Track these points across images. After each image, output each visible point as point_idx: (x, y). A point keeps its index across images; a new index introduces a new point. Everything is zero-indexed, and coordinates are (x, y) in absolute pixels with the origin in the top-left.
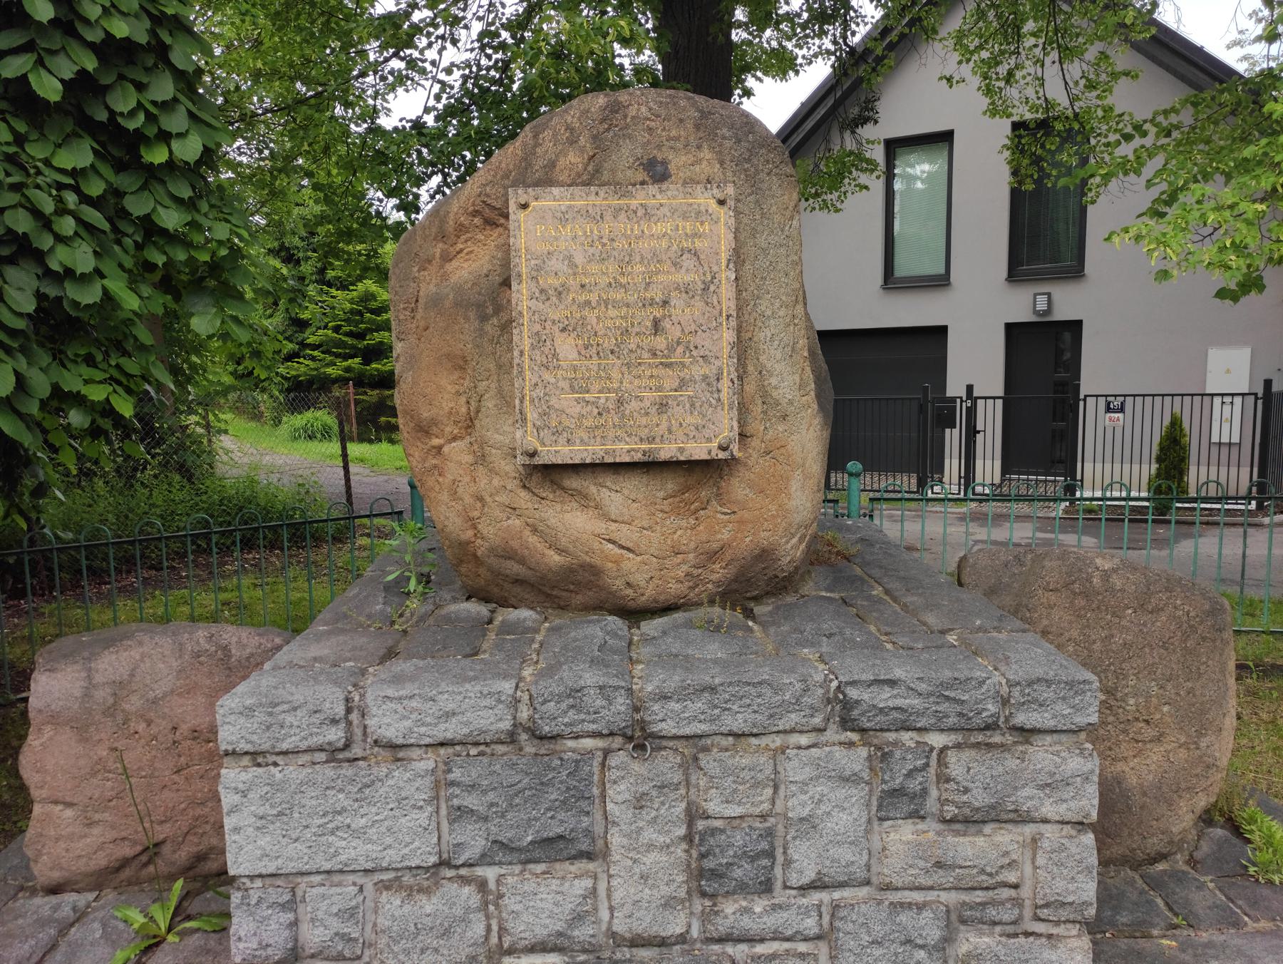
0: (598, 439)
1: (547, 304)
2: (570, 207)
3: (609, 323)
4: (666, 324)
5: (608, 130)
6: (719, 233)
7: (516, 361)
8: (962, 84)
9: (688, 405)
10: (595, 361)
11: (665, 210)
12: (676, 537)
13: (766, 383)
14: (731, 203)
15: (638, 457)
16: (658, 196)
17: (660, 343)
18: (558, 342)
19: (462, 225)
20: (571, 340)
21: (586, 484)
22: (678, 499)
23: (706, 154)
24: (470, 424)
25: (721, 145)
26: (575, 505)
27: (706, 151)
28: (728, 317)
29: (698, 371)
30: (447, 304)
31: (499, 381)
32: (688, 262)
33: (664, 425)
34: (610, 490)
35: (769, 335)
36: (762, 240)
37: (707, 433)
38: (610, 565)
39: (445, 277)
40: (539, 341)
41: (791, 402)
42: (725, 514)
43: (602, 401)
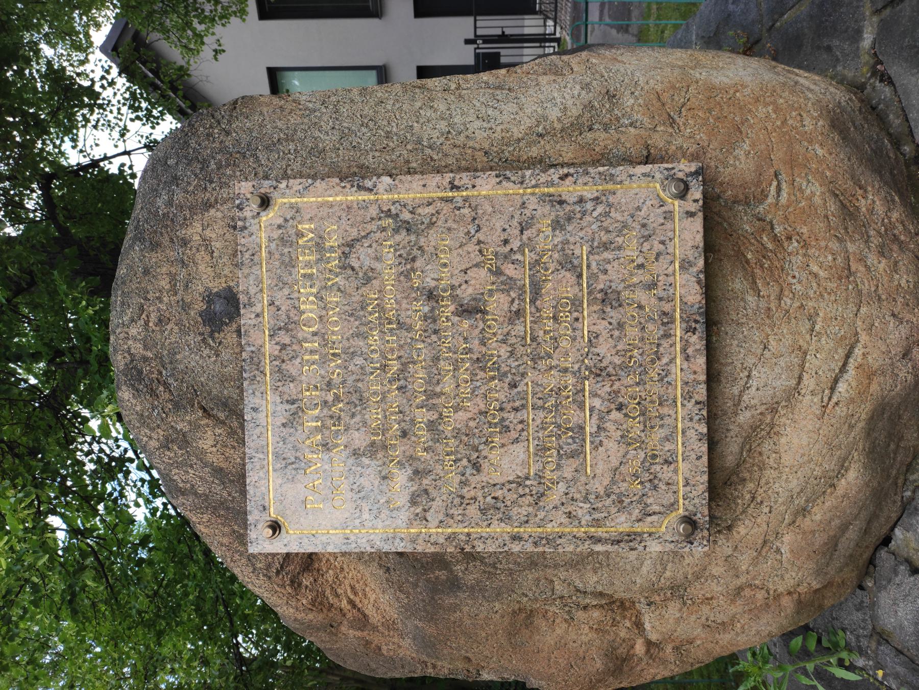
0: (665, 410)
1: (433, 493)
2: (277, 455)
3: (466, 389)
4: (466, 293)
5: (166, 385)
6: (316, 205)
7: (529, 547)
8: (221, 41)
9: (607, 255)
10: (529, 415)
11: (280, 297)
12: (822, 274)
13: (558, 126)
14: (266, 186)
15: (697, 341)
16: (258, 308)
17: (498, 304)
18: (497, 478)
19: (313, 602)
20: (494, 456)
21: (734, 429)
22: (758, 271)
23: (194, 231)
24: (618, 606)
25: (181, 207)
26: (767, 446)
27: (190, 231)
28: (454, 187)
29: (546, 237)
30: (431, 630)
31: (556, 566)
32: (362, 257)
33: (641, 296)
34: (746, 387)
35: (478, 123)
36: (328, 140)
37: (655, 218)
38: (874, 387)
39: (390, 625)
40: (494, 509)
41: (586, 86)
42: (779, 189)
43: (597, 403)
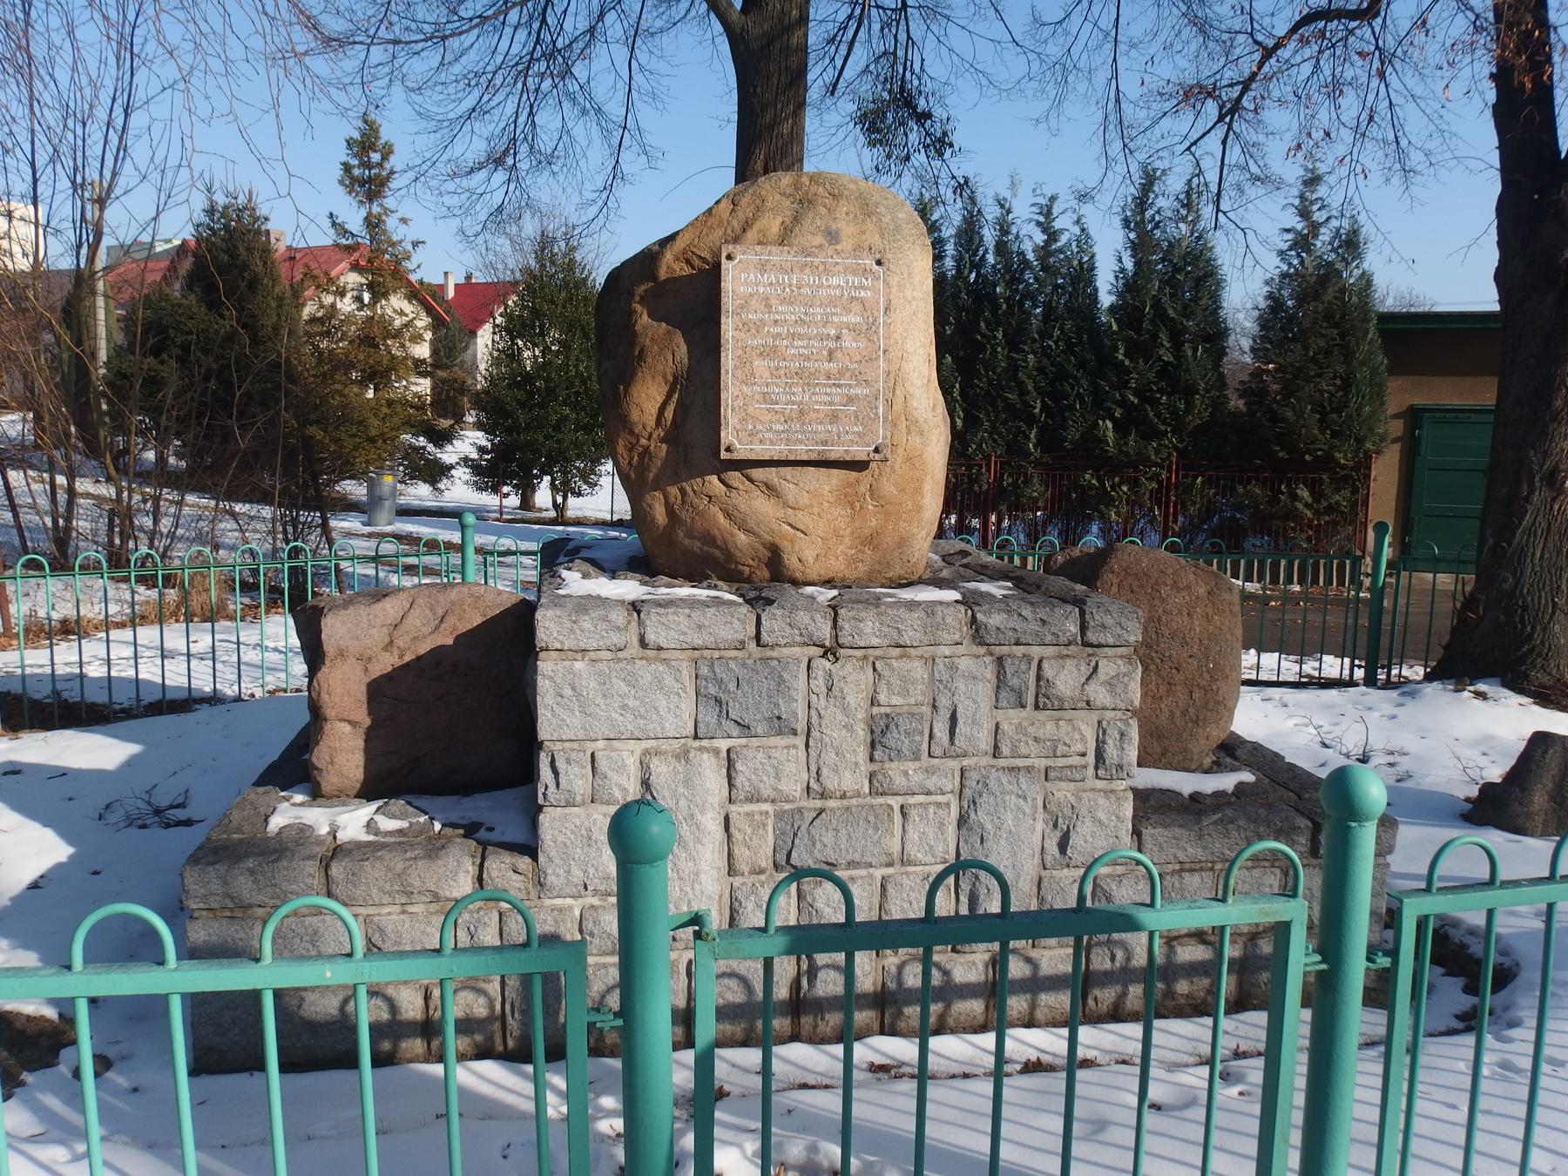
11: (840, 268)
15: (814, 457)
32: (856, 307)
40: (742, 363)
